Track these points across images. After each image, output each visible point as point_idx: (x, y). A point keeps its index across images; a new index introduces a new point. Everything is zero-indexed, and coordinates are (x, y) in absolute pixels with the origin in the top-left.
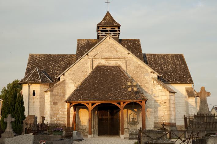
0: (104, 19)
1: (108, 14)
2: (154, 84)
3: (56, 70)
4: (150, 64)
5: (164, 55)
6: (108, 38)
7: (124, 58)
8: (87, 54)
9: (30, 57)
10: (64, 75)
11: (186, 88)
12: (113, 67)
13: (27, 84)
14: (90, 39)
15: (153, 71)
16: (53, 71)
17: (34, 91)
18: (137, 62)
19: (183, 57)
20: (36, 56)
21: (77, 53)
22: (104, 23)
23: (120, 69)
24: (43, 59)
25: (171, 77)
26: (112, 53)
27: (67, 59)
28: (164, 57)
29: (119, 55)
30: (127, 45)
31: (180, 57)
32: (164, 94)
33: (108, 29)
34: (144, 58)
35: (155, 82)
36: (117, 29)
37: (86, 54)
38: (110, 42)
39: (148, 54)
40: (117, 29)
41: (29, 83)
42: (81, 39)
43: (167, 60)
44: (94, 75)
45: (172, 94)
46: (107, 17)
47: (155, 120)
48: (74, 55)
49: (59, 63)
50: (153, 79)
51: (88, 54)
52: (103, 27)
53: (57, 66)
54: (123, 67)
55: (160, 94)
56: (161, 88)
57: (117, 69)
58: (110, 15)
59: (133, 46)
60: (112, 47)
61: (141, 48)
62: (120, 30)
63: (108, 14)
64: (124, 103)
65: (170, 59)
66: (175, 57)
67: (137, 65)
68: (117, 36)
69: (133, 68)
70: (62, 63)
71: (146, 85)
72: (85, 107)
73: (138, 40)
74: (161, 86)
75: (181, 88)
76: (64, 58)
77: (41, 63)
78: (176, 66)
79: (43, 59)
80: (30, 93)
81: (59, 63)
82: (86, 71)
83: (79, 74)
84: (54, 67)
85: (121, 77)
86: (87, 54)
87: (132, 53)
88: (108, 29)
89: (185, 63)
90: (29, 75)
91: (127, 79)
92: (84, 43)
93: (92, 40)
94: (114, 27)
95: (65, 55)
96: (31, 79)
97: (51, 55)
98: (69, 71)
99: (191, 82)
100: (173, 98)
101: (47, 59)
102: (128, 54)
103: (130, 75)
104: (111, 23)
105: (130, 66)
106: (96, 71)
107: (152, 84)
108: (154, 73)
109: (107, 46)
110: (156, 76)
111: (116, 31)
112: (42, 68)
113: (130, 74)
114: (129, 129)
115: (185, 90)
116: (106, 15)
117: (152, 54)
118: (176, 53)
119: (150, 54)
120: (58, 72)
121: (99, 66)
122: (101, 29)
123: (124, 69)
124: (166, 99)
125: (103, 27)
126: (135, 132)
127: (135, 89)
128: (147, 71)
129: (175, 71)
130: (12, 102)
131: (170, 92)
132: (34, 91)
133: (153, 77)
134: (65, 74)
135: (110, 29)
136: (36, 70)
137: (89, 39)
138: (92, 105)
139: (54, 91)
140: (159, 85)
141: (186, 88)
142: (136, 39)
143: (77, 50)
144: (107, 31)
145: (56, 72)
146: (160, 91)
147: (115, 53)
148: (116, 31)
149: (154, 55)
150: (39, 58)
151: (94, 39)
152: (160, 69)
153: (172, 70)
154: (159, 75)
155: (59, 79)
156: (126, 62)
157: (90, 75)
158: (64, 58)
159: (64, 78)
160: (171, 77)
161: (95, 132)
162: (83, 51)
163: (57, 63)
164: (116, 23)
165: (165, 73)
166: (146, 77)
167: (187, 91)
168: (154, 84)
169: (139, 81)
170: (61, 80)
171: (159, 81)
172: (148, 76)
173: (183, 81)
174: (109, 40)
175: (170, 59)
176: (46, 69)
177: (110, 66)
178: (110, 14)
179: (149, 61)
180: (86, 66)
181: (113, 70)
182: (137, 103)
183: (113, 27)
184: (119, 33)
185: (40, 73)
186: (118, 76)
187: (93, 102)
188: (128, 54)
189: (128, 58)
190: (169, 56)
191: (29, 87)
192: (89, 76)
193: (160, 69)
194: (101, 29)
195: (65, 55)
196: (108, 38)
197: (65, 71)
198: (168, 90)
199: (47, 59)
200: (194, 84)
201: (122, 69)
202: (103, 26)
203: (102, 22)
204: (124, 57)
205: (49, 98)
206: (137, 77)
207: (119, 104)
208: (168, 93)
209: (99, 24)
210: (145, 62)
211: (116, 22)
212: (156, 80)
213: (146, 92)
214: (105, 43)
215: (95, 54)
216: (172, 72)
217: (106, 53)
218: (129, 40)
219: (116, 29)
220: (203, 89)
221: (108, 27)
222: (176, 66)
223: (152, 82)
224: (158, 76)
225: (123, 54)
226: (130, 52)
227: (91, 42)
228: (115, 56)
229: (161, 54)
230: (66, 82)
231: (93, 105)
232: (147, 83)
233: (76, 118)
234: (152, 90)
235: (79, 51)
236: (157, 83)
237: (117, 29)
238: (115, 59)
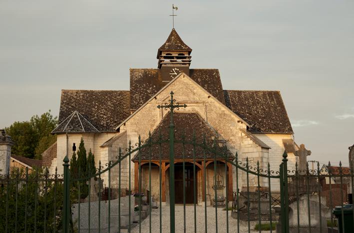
0: (169, 40)
1: (174, 33)
2: (242, 137)
3: (101, 114)
4: (234, 105)
5: (253, 93)
6: (182, 76)
7: (204, 102)
8: (155, 98)
9: (63, 94)
10: (125, 124)
11: (283, 140)
12: (189, 114)
13: (65, 135)
14: (148, 68)
15: (241, 120)
16: (97, 116)
17: (74, 144)
18: (220, 109)
19: (280, 95)
20: (72, 94)
21: (131, 90)
22: (169, 46)
23: (198, 117)
24: (81, 97)
25: (262, 125)
26: (188, 96)
27: (116, 97)
28: (253, 95)
29: (197, 98)
30: (201, 78)
31: (275, 96)
32: (255, 150)
33: (175, 54)
34: (226, 98)
35: (243, 134)
36: (188, 55)
37: (153, 97)
38: (185, 81)
39: (230, 91)
40: (188, 55)
41: (68, 133)
42: (136, 69)
43: (257, 99)
44: (166, 125)
45: (265, 150)
46: (173, 37)
47: (243, 183)
48: (125, 92)
49: (105, 104)
50: (242, 130)
51: (157, 97)
52: (167, 53)
53: (102, 109)
54: (203, 114)
55: (251, 150)
56: (251, 142)
57: (195, 117)
58: (177, 35)
59: (209, 80)
60: (187, 88)
61: (221, 83)
62: (191, 57)
63: (174, 33)
64: (206, 162)
65: (262, 98)
66: (269, 96)
67: (221, 112)
68: (188, 65)
69: (215, 116)
70: (109, 103)
71: (231, 138)
72: (155, 167)
73: (217, 71)
74: (251, 140)
75: (276, 141)
76: (112, 96)
77: (80, 104)
78: (269, 108)
79: (81, 97)
80: (69, 147)
81: (105, 104)
82: (154, 120)
83: (144, 124)
84: (98, 109)
85: (201, 128)
86: (155, 98)
87: (213, 96)
88: (175, 54)
89: (283, 103)
90: (66, 122)
91: (208, 130)
92: (140, 74)
93: (152, 70)
94: (183, 53)
95: (112, 92)
96: (70, 127)
97: (92, 92)
98: (132, 120)
99: (290, 131)
100: (266, 155)
101: (87, 98)
102: (209, 97)
103: (212, 126)
104: (178, 46)
105: (212, 113)
106: (168, 120)
107: (239, 137)
108: (242, 123)
109: (180, 86)
110: (244, 126)
111: (185, 58)
112: (82, 111)
113: (210, 124)
114: (210, 195)
115: (282, 143)
116: (172, 35)
117: (236, 91)
118: (270, 90)
119: (233, 91)
120: (105, 116)
121: (225, 149)
122: (163, 55)
123: (203, 117)
124: (258, 156)
125: (167, 53)
126: (220, 198)
127: (220, 145)
128: (232, 120)
129: (268, 115)
130: (82, 162)
131: (262, 148)
132: (74, 144)
133: (241, 128)
134: (127, 123)
135: (177, 55)
136: (76, 114)
137: (147, 69)
138: (166, 165)
139: (325, 191)
140: (249, 139)
141: (283, 140)
142: (213, 68)
143: (131, 85)
144: (173, 58)
145: (103, 117)
146: (250, 146)
147: (191, 96)
148: (185, 58)
149: (239, 92)
150: (76, 95)
151: (153, 68)
152: (247, 113)
153: (265, 113)
154: (248, 125)
155: (118, 130)
156: (206, 108)
157: (160, 126)
158: (112, 96)
159: (125, 128)
160: (262, 125)
161: (167, 199)
162: (140, 86)
163: (102, 103)
164: (186, 46)
165: (255, 119)
166: (231, 128)
167: (285, 144)
168: (242, 137)
169: (222, 133)
170: (121, 131)
171: (248, 133)
172: (234, 126)
173: (280, 130)
174: (183, 78)
175: (262, 98)
176: (91, 112)
177: (185, 114)
178: (176, 33)
179: (232, 102)
180: (153, 113)
181: (190, 118)
182: (223, 160)
183: (181, 53)
184: (190, 61)
185: (82, 119)
186: (196, 126)
187: (168, 161)
188: (209, 97)
189: (208, 102)
190: (260, 94)
191: (67, 138)
192: (159, 127)
193: (247, 113)
194: (163, 55)
195: (112, 91)
196: (182, 76)
197: (126, 120)
198: (260, 145)
199: (87, 98)
200: (294, 135)
201: (201, 117)
202: (168, 51)
203: (165, 44)
204: (204, 101)
205: (107, 155)
206: (220, 128)
207: (200, 163)
208: (260, 148)
209: (161, 48)
210: (227, 104)
211: (185, 45)
212: (244, 132)
213: (232, 148)
214: (178, 83)
215: (165, 98)
216: (264, 118)
217: (180, 95)
218: (203, 70)
219: (186, 55)
220: (302, 146)
221: (175, 50)
222: (269, 108)
223: (240, 135)
224: (247, 126)
225: (203, 97)
226: (211, 95)
227: (150, 73)
228: (192, 100)
229: (248, 91)
230: (128, 134)
231: (167, 164)
232: (233, 135)
233: (142, 181)
234: (240, 144)
235: (133, 86)
236: (246, 135)
237: (186, 55)
238: (191, 104)
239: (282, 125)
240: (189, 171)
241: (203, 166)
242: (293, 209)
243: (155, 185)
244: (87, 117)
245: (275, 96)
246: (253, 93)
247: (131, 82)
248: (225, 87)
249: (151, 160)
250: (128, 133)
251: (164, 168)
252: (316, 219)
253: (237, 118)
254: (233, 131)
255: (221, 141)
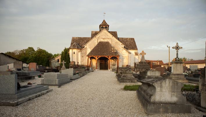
0: (103, 23)
1: (104, 21)
12: (106, 42)
18: (116, 41)
28: (126, 39)
29: (109, 37)
31: (133, 39)
32: (126, 53)
33: (104, 27)
45: (129, 54)
54: (110, 42)
57: (108, 43)
59: (114, 34)
63: (104, 21)
72: (94, 58)
75: (133, 52)
88: (104, 27)
91: (112, 47)
95: (86, 38)
99: (137, 49)
110: (123, 46)
113: (113, 45)
116: (103, 21)
122: (101, 27)
128: (120, 44)
129: (131, 45)
144: (104, 28)
147: (107, 36)
149: (123, 38)
153: (130, 44)
155: (84, 47)
167: (135, 53)
176: (79, 43)
182: (115, 57)
185: (77, 45)
190: (129, 39)
194: (101, 27)
207: (108, 57)
208: (128, 53)
221: (104, 26)
231: (98, 57)
232: (120, 49)
237: (108, 27)
239: (134, 47)
240: (202, 66)
241: (110, 58)
242: (156, 87)
243: (94, 62)
244: (78, 45)
245: (133, 39)
246: (126, 38)
247: (92, 35)
248: (118, 37)
249: (93, 56)
250: (87, 48)
251: (97, 58)
252: (177, 97)
253: (121, 44)
254: (120, 48)
255: (115, 50)
